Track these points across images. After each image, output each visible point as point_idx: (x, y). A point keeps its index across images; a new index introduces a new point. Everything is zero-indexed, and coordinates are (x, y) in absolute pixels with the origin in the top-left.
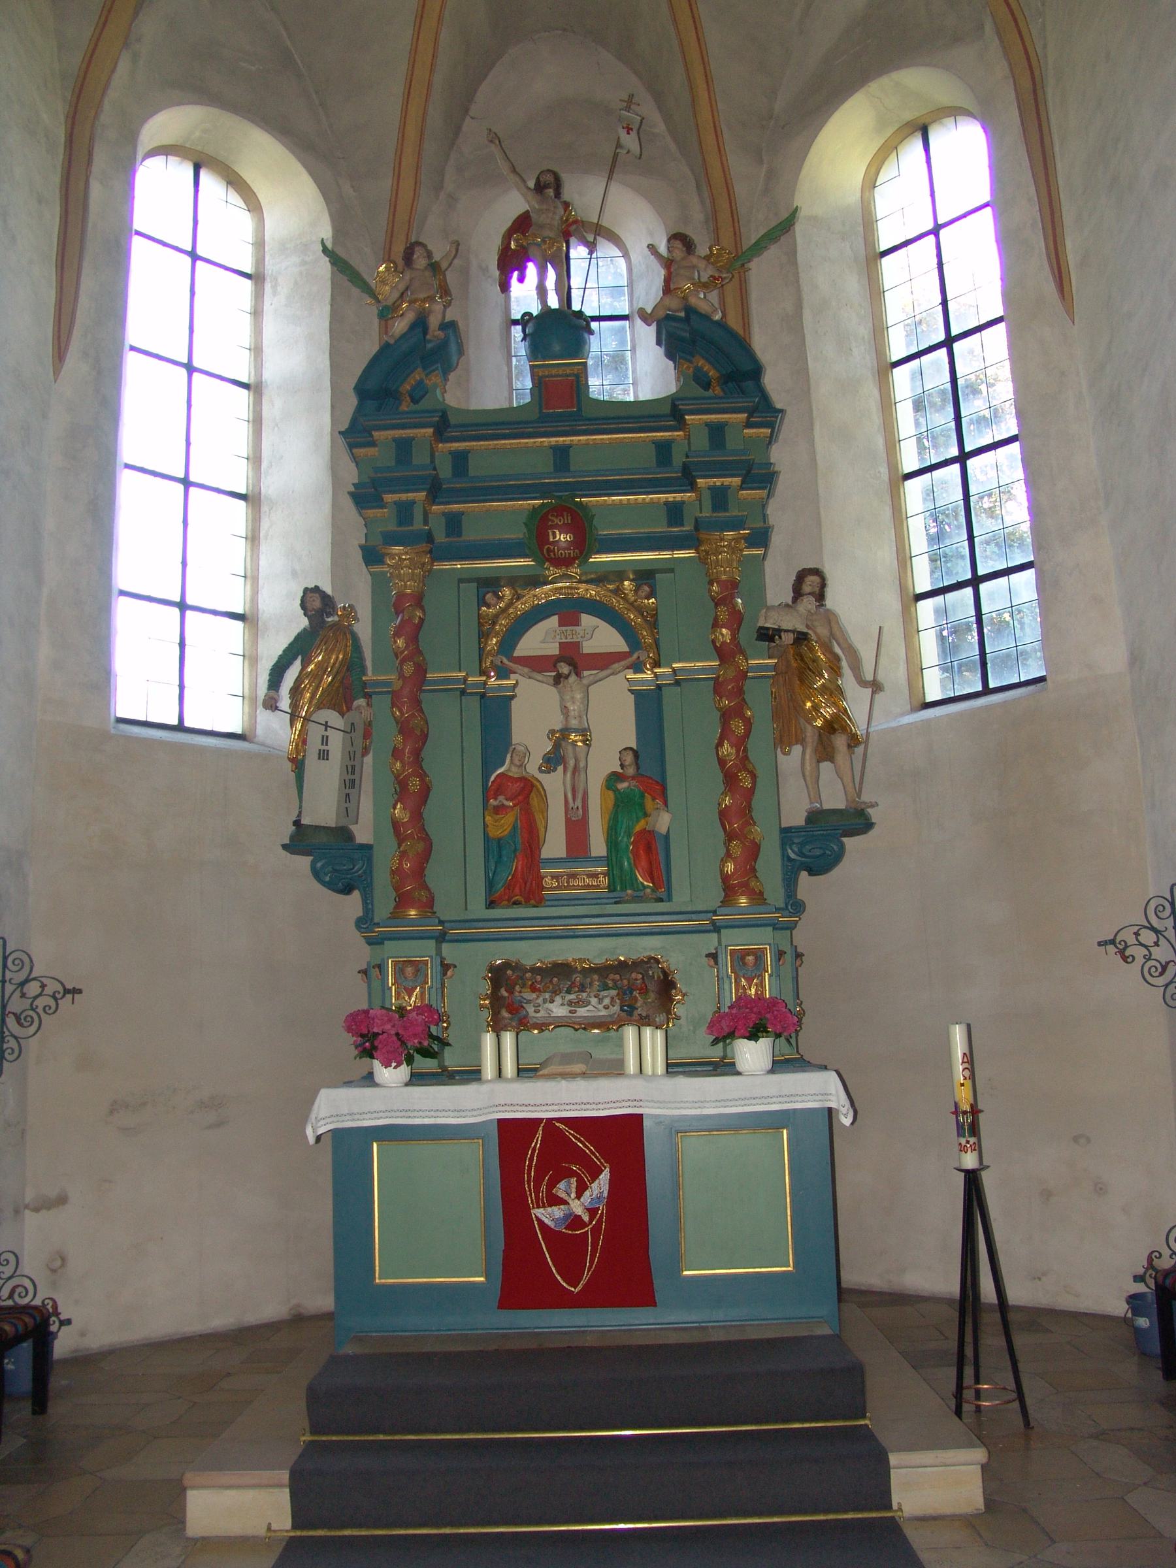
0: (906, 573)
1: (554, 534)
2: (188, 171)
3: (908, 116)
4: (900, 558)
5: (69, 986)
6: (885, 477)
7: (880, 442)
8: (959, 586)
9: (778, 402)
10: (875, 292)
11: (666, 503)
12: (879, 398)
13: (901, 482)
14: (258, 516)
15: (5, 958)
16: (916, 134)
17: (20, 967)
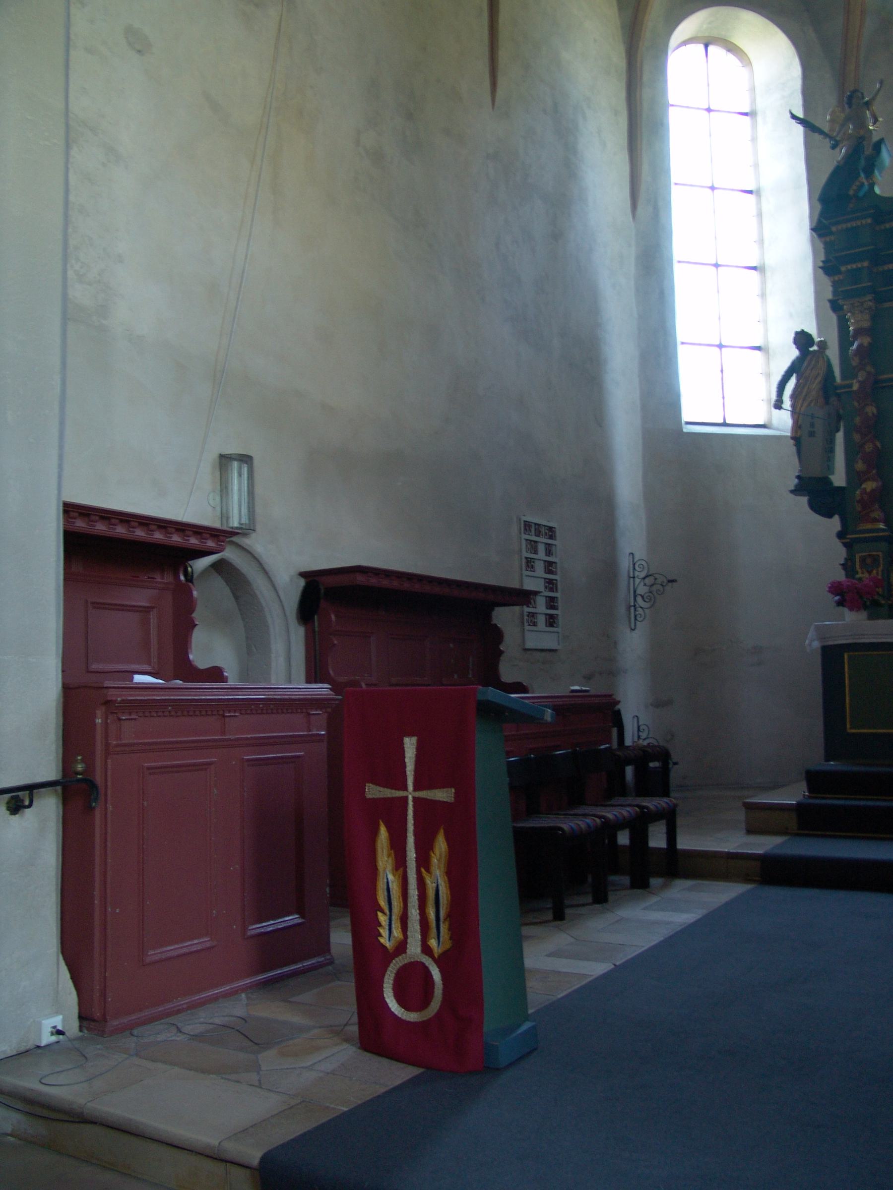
2: (701, 47)
5: (670, 578)
15: (634, 565)
17: (642, 569)
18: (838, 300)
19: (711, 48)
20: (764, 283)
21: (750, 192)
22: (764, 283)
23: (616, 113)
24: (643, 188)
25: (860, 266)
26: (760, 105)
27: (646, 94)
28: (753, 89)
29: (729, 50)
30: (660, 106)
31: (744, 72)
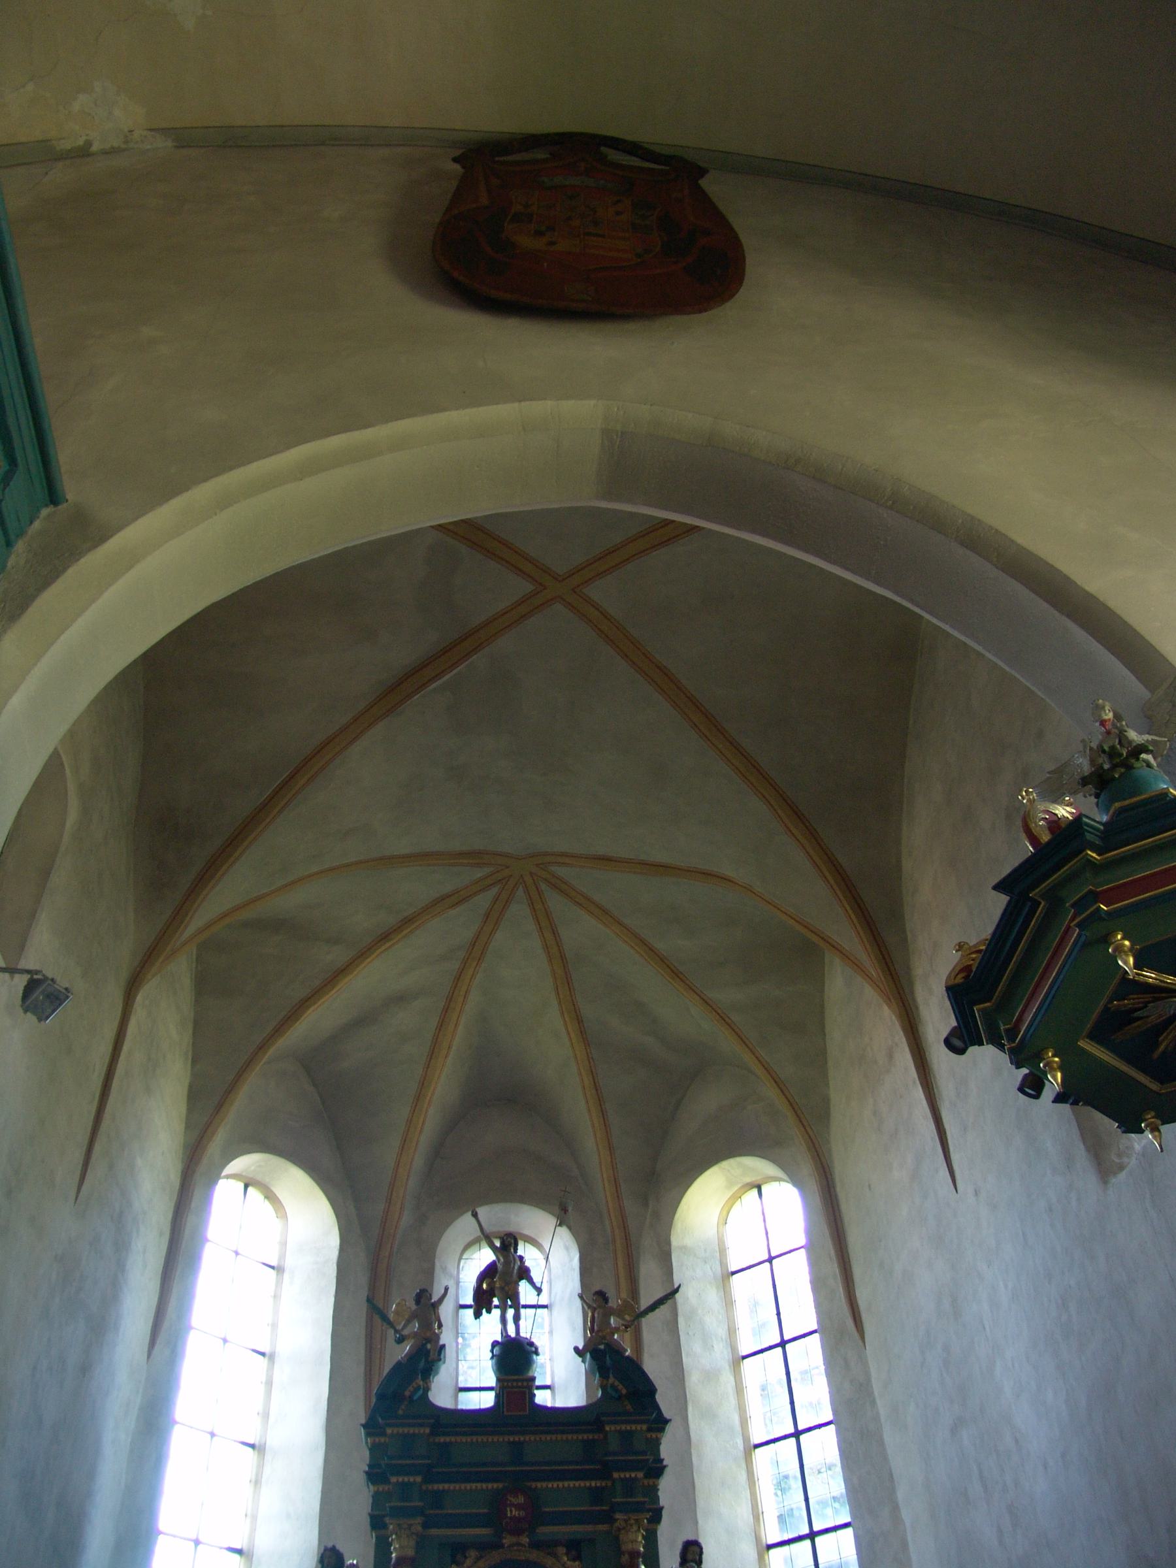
0: (759, 1526)
1: (511, 1511)
2: (242, 1185)
3: (748, 1180)
4: (754, 1513)
6: (741, 1446)
7: (736, 1419)
8: (800, 1538)
9: (667, 1414)
10: (728, 1302)
11: (590, 1488)
12: (734, 1384)
13: (753, 1450)
14: (262, 1463)
16: (754, 1189)
18: (384, 1516)
19: (250, 1189)
20: (260, 1466)
21: (263, 1354)
22: (260, 1466)
23: (161, 1234)
24: (166, 1324)
25: (412, 1480)
26: (289, 1263)
27: (191, 1220)
28: (284, 1244)
29: (266, 1197)
30: (199, 1239)
31: (277, 1223)
